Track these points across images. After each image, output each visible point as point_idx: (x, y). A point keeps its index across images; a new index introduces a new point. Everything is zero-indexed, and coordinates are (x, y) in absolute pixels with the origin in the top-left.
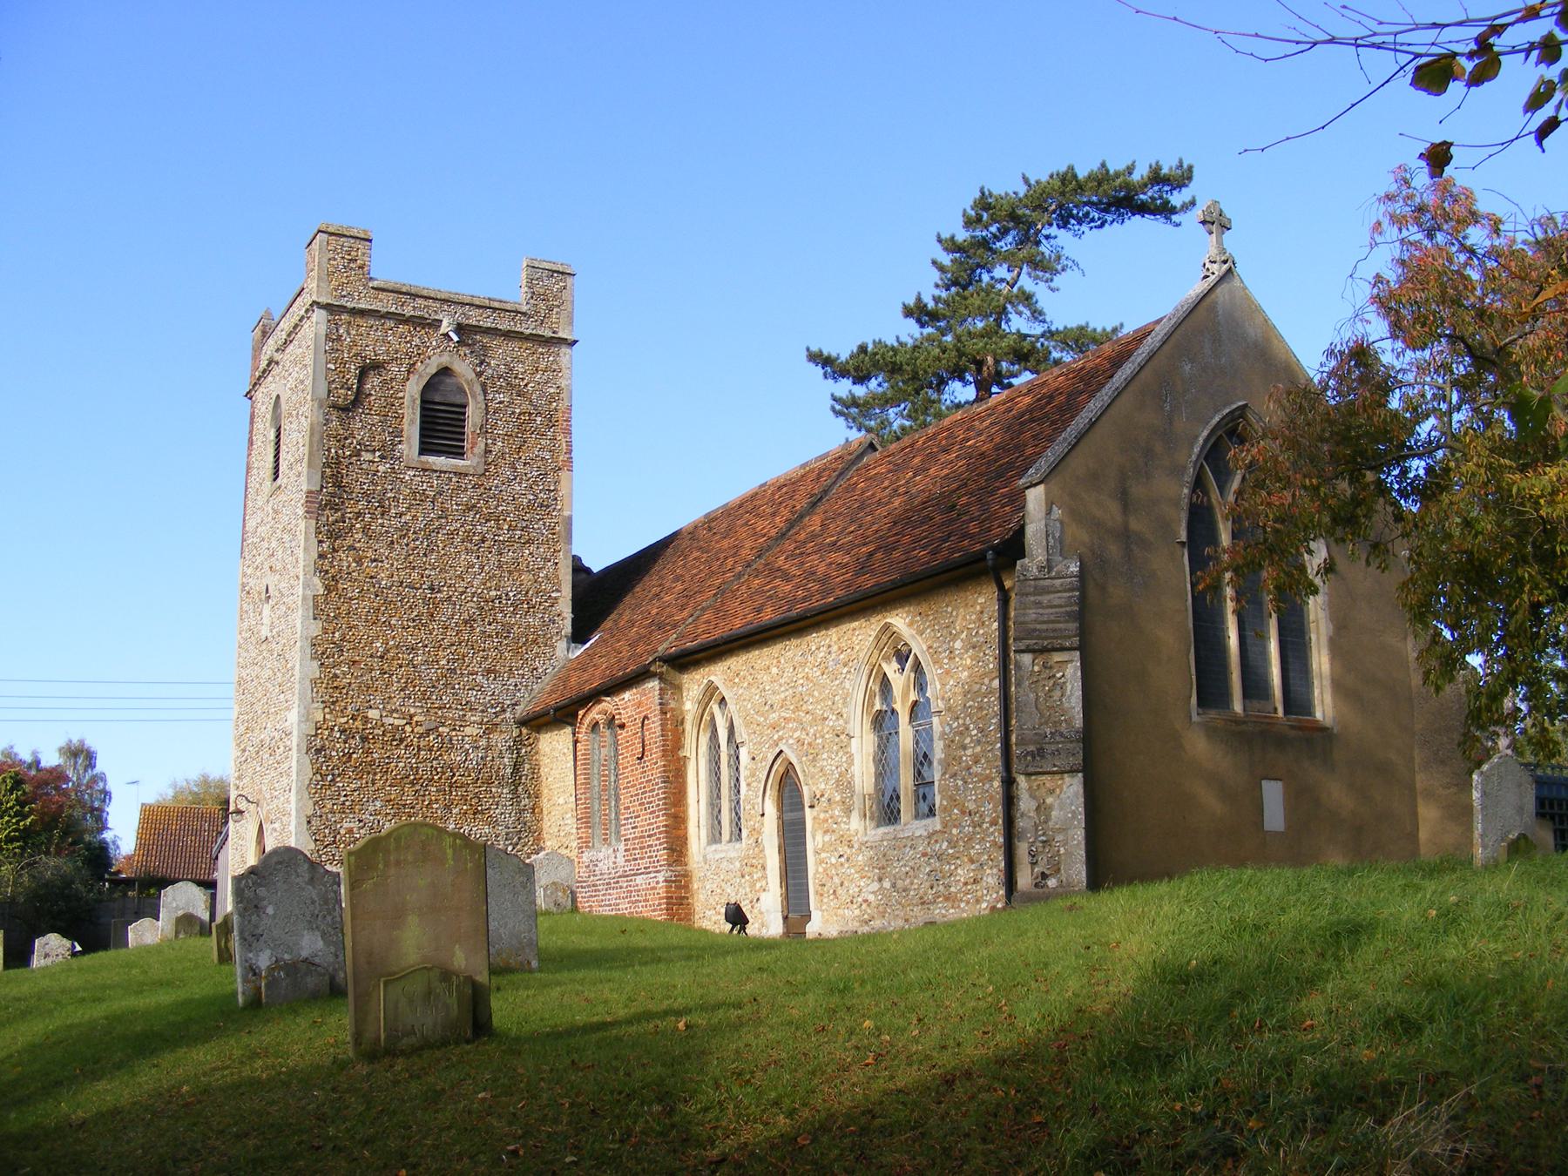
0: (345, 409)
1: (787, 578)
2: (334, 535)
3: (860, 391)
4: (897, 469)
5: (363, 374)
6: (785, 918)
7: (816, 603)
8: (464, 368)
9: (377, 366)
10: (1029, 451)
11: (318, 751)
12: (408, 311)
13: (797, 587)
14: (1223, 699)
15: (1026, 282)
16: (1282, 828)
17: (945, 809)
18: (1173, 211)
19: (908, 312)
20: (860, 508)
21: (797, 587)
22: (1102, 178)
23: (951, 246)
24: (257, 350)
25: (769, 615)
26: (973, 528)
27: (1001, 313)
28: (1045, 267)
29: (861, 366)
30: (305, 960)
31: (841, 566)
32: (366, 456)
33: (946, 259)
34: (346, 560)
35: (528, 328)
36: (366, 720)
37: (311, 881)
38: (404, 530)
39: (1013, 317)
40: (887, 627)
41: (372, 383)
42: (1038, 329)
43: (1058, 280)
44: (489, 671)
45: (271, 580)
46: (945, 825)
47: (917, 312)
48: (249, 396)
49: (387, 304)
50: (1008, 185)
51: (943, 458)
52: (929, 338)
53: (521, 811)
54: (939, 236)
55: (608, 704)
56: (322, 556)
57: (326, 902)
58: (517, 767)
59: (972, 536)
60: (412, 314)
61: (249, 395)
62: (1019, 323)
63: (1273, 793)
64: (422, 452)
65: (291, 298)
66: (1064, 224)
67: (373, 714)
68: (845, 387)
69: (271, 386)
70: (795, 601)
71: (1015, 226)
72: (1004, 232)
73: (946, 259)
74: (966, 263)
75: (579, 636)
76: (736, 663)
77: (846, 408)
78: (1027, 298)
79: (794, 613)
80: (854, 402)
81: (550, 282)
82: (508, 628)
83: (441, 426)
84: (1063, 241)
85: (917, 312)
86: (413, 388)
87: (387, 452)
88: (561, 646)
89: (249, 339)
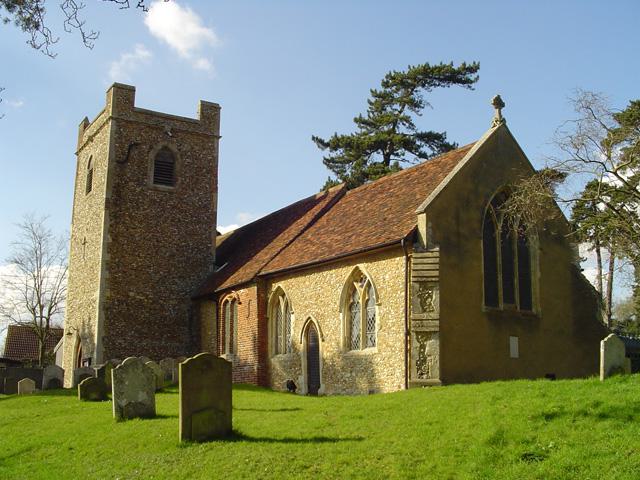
0: (122, 163)
1: (313, 244)
2: (116, 217)
3: (334, 155)
4: (360, 199)
5: (131, 147)
6: (309, 387)
7: (327, 256)
8: (174, 148)
9: (136, 144)
10: (418, 197)
11: (107, 309)
12: (151, 122)
13: (318, 248)
14: (496, 304)
15: (407, 112)
16: (517, 356)
17: (380, 344)
18: (472, 82)
19: (356, 120)
20: (343, 216)
21: (318, 248)
22: (439, 69)
23: (374, 93)
24: (81, 135)
25: (306, 261)
26: (395, 228)
27: (395, 124)
28: (415, 105)
29: (335, 144)
30: (140, 403)
31: (337, 241)
32: (131, 184)
33: (373, 100)
34: (122, 228)
35: (201, 131)
36: (129, 296)
37: (143, 371)
38: (146, 216)
39: (401, 126)
40: (357, 268)
41: (135, 153)
42: (412, 133)
43: (422, 111)
44: (180, 277)
45: (87, 235)
46: (379, 351)
47: (359, 121)
48: (77, 154)
49: (142, 119)
50: (403, 68)
51: (380, 196)
52: (365, 134)
53: (192, 337)
54: (313, 138)
55: (234, 294)
56: (111, 226)
57: (148, 379)
58: (191, 319)
59: (394, 233)
60: (157, 122)
61: (77, 154)
62: (402, 129)
63: (514, 342)
64: (155, 182)
65: (98, 113)
66: (423, 86)
67: (131, 294)
68: (327, 153)
69: (90, 151)
70: (317, 255)
71: (409, 84)
72: (398, 90)
73: (373, 100)
74: (382, 100)
75: (218, 263)
76: (292, 281)
77: (328, 162)
78: (407, 119)
79: (317, 260)
80: (332, 160)
81: (211, 111)
82: (189, 259)
83: (165, 171)
84: (421, 93)
85: (359, 121)
86: (152, 156)
87: (140, 183)
88: (211, 267)
89: (77, 129)
